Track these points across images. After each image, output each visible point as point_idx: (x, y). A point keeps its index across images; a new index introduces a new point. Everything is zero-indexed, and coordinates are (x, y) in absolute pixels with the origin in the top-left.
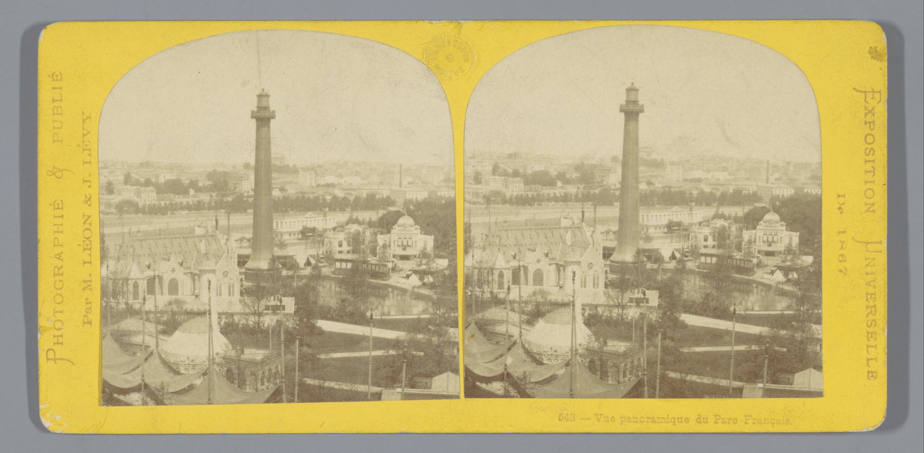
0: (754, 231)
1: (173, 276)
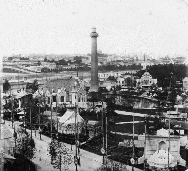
0: (140, 79)
1: (62, 95)
